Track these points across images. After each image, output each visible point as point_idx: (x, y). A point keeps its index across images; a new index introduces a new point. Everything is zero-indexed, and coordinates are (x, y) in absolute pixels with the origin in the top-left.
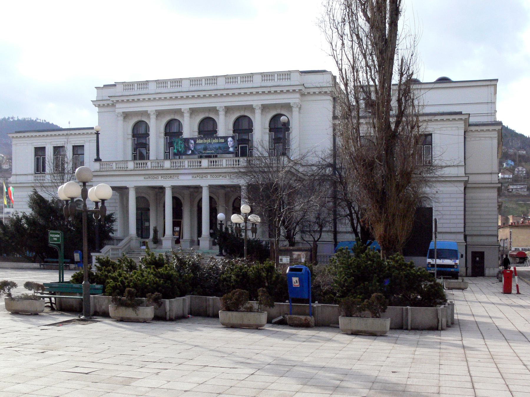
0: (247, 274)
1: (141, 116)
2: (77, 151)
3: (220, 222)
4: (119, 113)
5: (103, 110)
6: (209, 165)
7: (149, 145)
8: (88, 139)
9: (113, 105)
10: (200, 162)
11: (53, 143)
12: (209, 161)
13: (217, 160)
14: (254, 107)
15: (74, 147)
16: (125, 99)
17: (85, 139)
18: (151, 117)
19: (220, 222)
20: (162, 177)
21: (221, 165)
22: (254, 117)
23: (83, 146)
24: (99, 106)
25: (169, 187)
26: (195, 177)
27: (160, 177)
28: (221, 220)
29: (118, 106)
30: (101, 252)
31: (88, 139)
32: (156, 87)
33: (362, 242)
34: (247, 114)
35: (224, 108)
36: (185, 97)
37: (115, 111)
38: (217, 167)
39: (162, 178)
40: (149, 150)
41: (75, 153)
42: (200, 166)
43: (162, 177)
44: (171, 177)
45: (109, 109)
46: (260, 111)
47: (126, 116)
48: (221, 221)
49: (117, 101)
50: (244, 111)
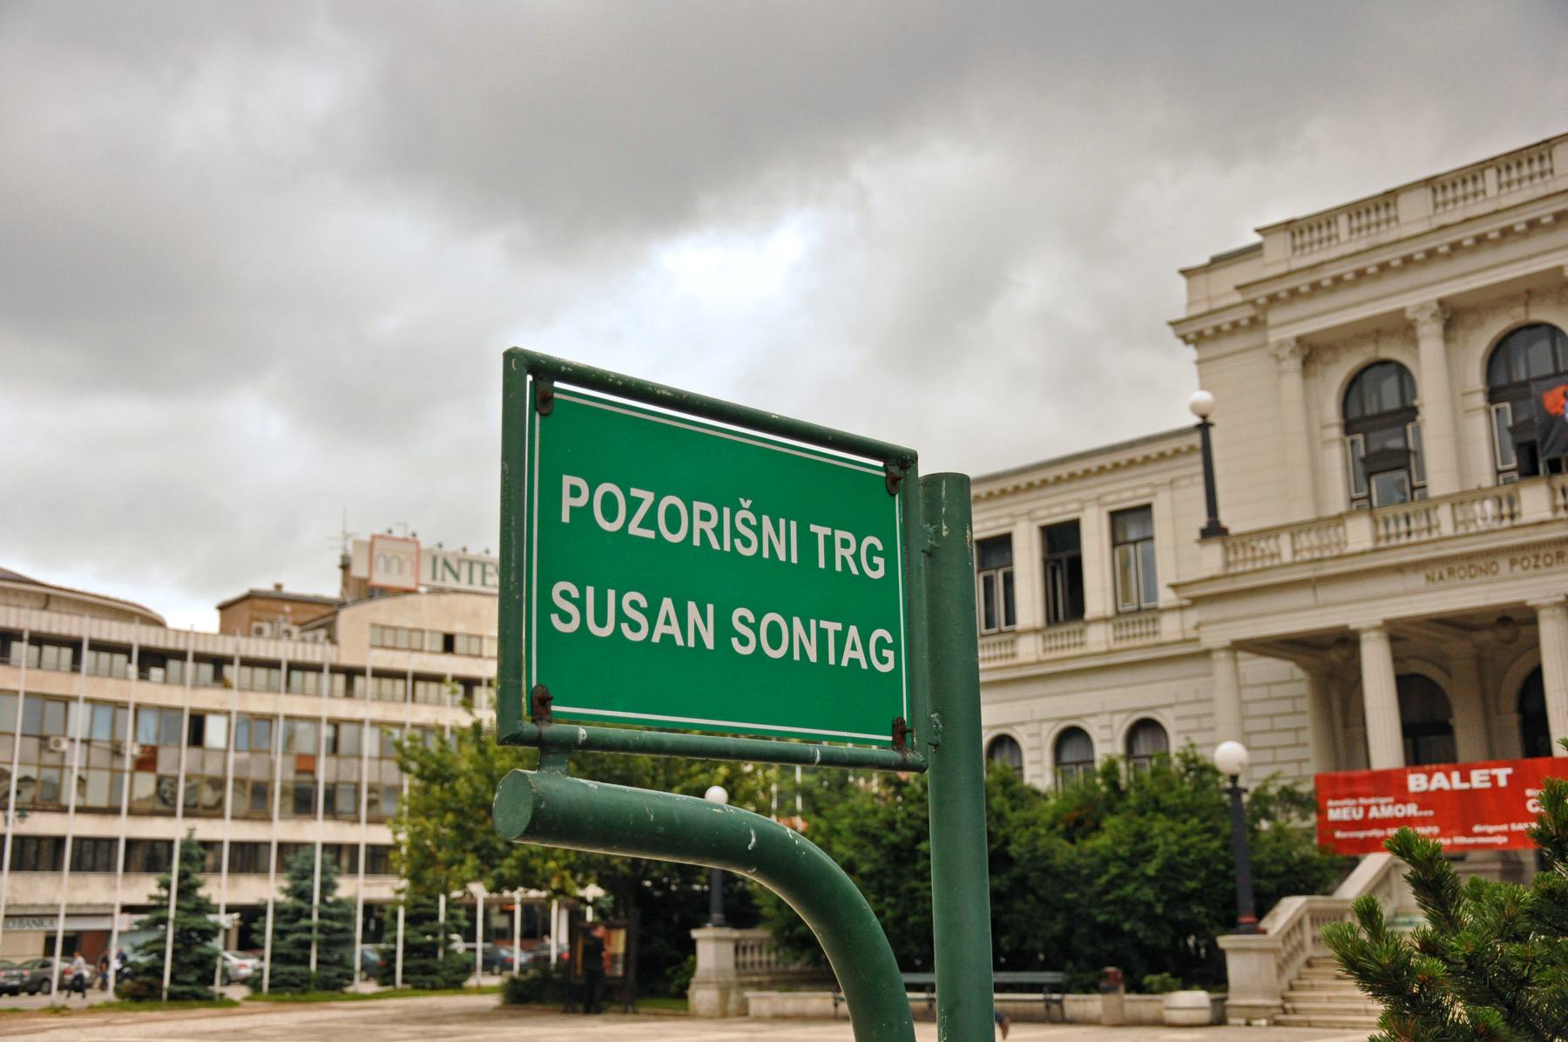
0: (1428, 941)
1: (1527, 304)
2: (1125, 532)
3: (1229, 785)
4: (1281, 344)
5: (1212, 350)
6: (1377, 539)
7: (1419, 454)
8: (1168, 477)
9: (1255, 323)
10: (1511, 502)
11: (1110, 499)
12: (1553, 491)
13: (1390, 515)
14: (1409, 315)
15: (1116, 516)
16: (1303, 283)
17: (1155, 479)
18: (1422, 330)
19: (1229, 785)
20: (1513, 563)
21: (1338, 544)
22: (1417, 358)
23: (1147, 508)
24: (1198, 339)
25: (1377, 628)
26: (1441, 578)
27: (1504, 564)
28: (1236, 769)
29: (1274, 317)
30: (1264, 932)
31: (1168, 477)
32: (1431, 205)
33: (1426, 793)
34: (1389, 351)
35: (1435, 306)
36: (1396, 263)
37: (1265, 344)
38: (1414, 538)
39: (1517, 568)
40: (1422, 476)
41: (1120, 538)
42: (1512, 516)
43: (1513, 563)
44: (1451, 572)
45: (1242, 341)
46: (1436, 328)
47: (1311, 353)
48: (1234, 778)
49: (1273, 299)
50: (1527, 304)
